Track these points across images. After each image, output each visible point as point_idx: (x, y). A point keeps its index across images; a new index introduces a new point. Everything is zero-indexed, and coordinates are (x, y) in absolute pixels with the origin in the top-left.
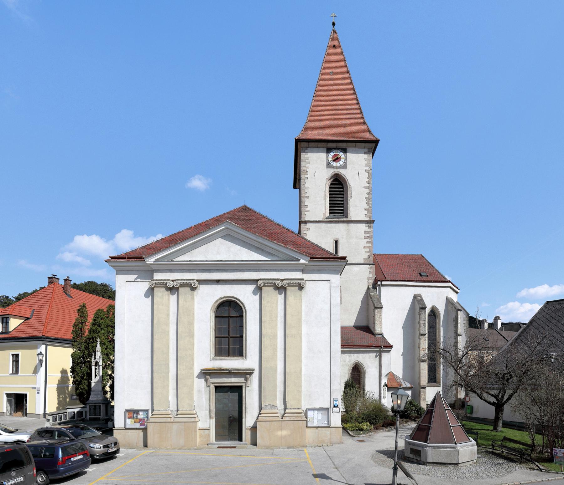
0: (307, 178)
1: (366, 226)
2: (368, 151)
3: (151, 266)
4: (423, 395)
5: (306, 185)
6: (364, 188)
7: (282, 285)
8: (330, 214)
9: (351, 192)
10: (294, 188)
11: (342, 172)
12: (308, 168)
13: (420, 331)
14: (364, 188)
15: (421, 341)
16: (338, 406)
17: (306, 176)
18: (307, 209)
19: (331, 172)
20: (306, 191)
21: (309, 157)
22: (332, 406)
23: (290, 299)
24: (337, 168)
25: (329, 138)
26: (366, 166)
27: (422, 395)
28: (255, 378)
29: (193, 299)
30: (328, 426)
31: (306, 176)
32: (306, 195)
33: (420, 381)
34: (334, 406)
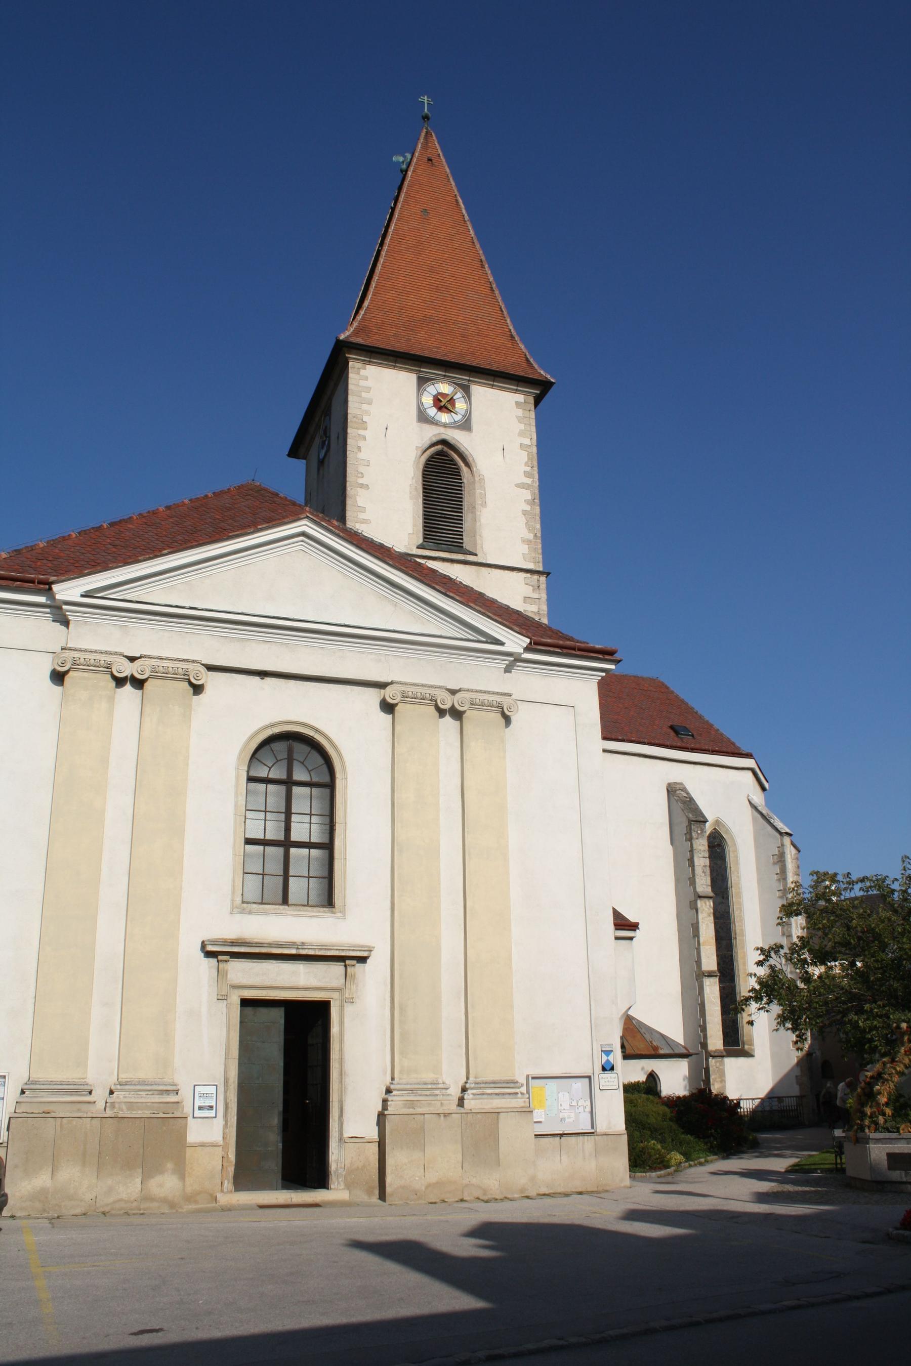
0: (364, 438)
1: (527, 584)
2: (525, 400)
3: (64, 607)
4: (718, 1080)
5: (361, 456)
6: (518, 486)
7: (453, 706)
8: (425, 538)
9: (485, 491)
10: (289, 455)
11: (457, 437)
12: (368, 413)
13: (695, 888)
14: (518, 486)
15: (700, 916)
16: (612, 1069)
17: (361, 432)
18: (362, 516)
19: (431, 434)
20: (362, 469)
21: (370, 388)
22: (598, 1068)
23: (475, 747)
24: (445, 426)
25: (426, 354)
26: (521, 434)
27: (715, 1080)
28: (376, 970)
29: (187, 717)
30: (593, 1131)
31: (361, 432)
32: (361, 481)
33: (705, 1037)
34: (604, 1069)
